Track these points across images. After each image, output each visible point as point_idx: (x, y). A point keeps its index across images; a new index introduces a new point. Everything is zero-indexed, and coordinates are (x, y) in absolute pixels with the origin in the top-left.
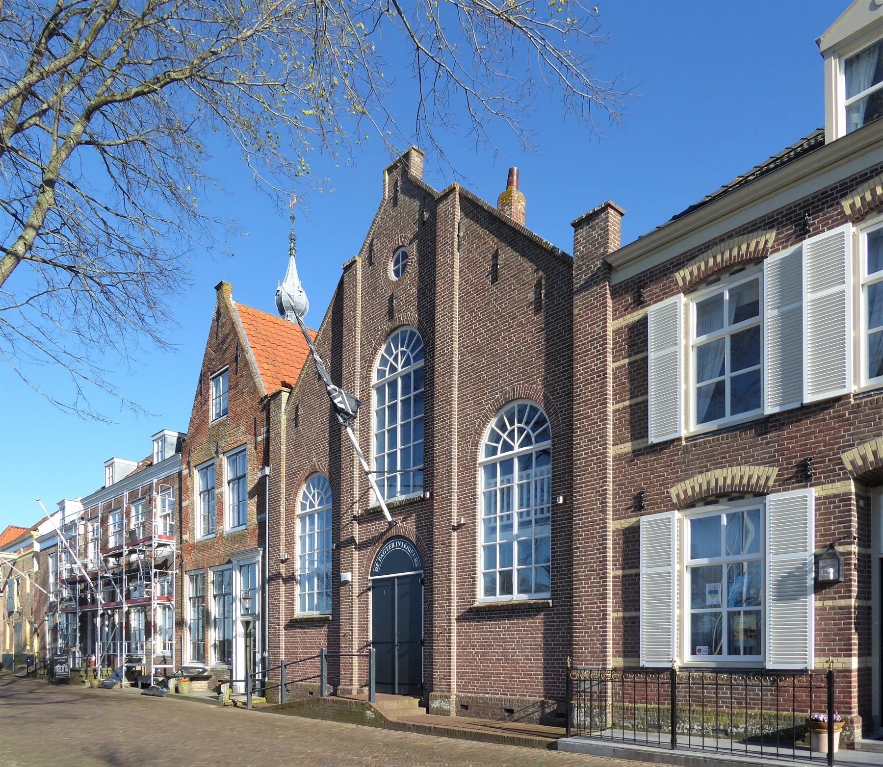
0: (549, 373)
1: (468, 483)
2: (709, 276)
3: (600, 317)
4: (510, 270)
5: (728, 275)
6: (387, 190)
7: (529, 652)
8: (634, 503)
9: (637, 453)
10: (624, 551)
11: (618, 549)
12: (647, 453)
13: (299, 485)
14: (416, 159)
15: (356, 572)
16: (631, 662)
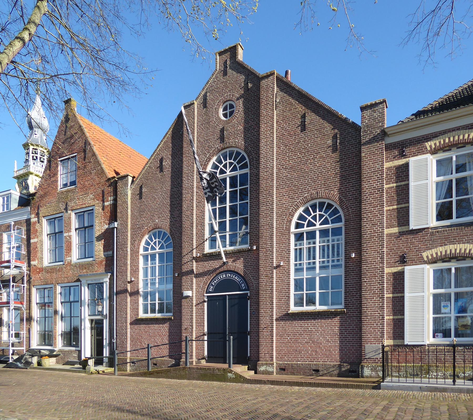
0: (343, 186)
1: (284, 243)
2: (445, 147)
3: (379, 160)
4: (314, 126)
5: (456, 148)
6: (218, 65)
7: (329, 338)
8: (400, 259)
9: (401, 234)
10: (393, 284)
11: (389, 283)
12: (408, 234)
13: (143, 236)
14: (240, 51)
15: (194, 291)
16: (398, 342)
